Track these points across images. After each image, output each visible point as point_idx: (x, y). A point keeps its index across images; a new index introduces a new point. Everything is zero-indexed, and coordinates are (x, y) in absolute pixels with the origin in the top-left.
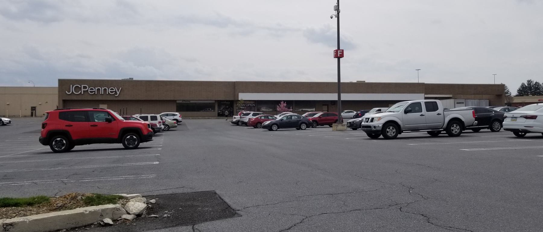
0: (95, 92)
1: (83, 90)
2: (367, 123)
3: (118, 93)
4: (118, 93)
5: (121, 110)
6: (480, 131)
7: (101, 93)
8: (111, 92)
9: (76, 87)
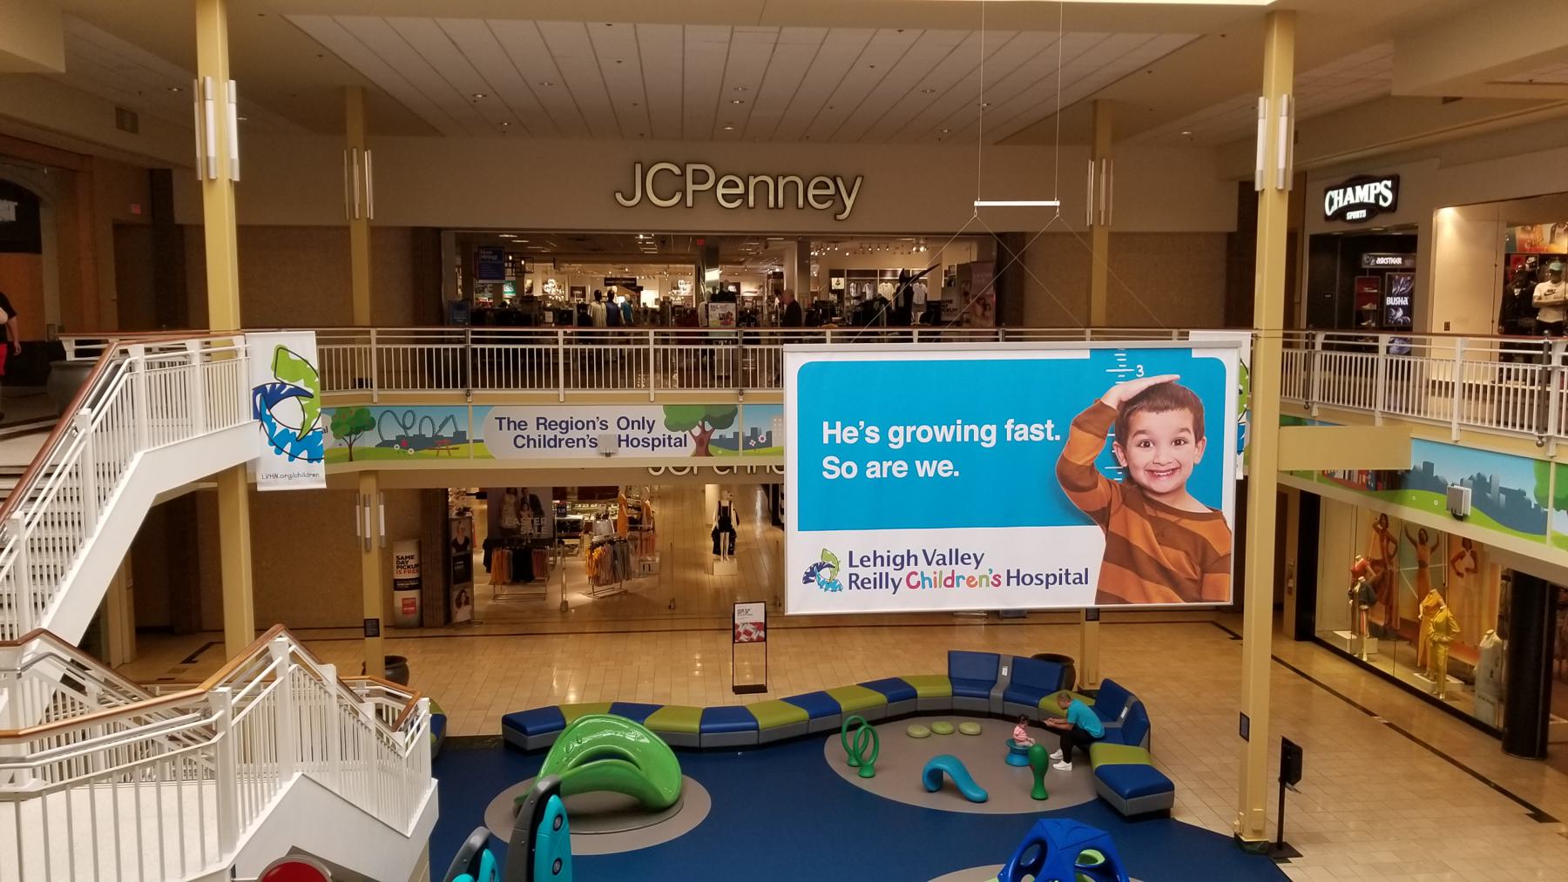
1: (691, 187)
3: (849, 203)
7: (772, 204)
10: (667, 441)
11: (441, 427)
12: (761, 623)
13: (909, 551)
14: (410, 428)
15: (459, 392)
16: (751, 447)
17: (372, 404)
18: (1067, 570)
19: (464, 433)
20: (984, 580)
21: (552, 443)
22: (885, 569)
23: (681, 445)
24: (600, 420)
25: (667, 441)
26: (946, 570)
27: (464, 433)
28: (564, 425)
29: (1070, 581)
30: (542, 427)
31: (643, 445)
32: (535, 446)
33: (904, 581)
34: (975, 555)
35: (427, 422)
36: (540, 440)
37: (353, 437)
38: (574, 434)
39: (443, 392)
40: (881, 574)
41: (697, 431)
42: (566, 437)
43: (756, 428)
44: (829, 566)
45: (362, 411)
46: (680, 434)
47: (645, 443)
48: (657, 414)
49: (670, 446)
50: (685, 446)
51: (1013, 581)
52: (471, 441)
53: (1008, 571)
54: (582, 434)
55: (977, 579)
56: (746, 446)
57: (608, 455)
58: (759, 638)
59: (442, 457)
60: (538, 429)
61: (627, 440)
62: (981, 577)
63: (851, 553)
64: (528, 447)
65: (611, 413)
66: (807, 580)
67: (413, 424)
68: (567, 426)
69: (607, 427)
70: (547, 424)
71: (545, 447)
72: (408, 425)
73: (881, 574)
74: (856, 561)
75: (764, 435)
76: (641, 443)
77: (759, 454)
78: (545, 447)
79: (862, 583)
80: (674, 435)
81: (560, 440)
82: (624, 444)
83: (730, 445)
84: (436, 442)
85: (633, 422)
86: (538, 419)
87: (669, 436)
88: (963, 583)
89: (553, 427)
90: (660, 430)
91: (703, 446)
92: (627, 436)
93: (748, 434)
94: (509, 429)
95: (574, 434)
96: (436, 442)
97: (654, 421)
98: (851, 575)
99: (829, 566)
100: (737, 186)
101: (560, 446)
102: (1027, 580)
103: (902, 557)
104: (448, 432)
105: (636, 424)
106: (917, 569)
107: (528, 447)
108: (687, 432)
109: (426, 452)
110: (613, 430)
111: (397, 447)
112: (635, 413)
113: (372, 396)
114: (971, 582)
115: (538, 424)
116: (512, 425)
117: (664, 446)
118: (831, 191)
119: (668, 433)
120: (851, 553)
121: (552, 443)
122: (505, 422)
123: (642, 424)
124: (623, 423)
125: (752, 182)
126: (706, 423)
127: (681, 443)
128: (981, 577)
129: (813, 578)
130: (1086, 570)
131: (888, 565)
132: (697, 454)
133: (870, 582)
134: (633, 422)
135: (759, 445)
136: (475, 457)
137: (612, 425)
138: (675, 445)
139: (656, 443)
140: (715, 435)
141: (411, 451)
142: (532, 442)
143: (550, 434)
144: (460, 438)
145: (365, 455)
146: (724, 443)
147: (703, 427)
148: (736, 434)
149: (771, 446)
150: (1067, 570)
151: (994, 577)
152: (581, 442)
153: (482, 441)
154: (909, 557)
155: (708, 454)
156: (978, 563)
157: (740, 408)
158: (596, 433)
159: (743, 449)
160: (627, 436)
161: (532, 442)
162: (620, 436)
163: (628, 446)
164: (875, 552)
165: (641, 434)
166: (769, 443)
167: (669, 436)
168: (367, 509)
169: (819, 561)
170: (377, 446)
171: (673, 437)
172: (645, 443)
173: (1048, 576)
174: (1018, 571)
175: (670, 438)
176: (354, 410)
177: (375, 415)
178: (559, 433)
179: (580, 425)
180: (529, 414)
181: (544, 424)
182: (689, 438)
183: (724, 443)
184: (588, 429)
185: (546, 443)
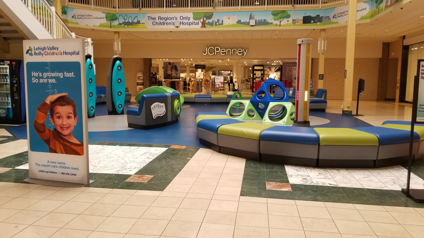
1: (216, 52)
3: (245, 54)
4: (245, 54)
8: (239, 52)
10: (193, 23)
11: (133, 20)
12: (223, 82)
13: (45, 47)
14: (126, 20)
15: (138, 9)
16: (217, 25)
17: (116, 13)
18: (75, 51)
19: (139, 21)
20: (59, 53)
21: (162, 24)
22: (40, 51)
23: (197, 24)
24: (175, 17)
25: (193, 23)
26: (52, 51)
27: (139, 21)
28: (165, 19)
29: (76, 54)
30: (160, 19)
31: (187, 25)
32: (158, 25)
33: (44, 53)
34: (57, 48)
35: (130, 18)
36: (159, 23)
37: (111, 21)
38: (168, 21)
39: (134, 9)
40: (40, 52)
41: (202, 20)
42: (166, 22)
43: (219, 19)
44: (31, 50)
45: (114, 15)
46: (197, 21)
47: (187, 24)
48: (191, 15)
49: (194, 24)
50: (199, 24)
51: (64, 54)
52: (141, 23)
53: (63, 51)
54: (170, 21)
55: (58, 53)
56: (216, 25)
57: (177, 27)
58: (222, 86)
59: (134, 28)
60: (159, 20)
61: (182, 23)
62: (58, 53)
63: (34, 47)
64: (156, 25)
65: (178, 15)
66: (27, 53)
67: (127, 19)
68: (167, 19)
69: (177, 19)
70: (161, 18)
71: (160, 25)
72: (126, 19)
73: (40, 52)
74: (35, 49)
75: (221, 21)
76: (186, 24)
77: (219, 27)
78: (160, 25)
79: (36, 54)
80: (195, 21)
81: (164, 23)
82: (181, 24)
83: (211, 24)
84: (132, 24)
85: (184, 18)
86: (159, 17)
87: (194, 22)
88: (55, 54)
89: (163, 19)
90: (192, 20)
91: (204, 24)
92: (183, 22)
93: (216, 21)
94: (151, 20)
95: (168, 21)
96: (132, 24)
97: (190, 18)
98: (34, 52)
99: (31, 50)
100: (224, 51)
101: (164, 25)
102: (67, 54)
103: (43, 48)
104: (135, 21)
105: (185, 18)
106: (46, 51)
107: (156, 25)
108: (199, 21)
109: (130, 26)
110: (179, 20)
111: (123, 25)
112: (185, 15)
113: (116, 11)
114: (56, 54)
115: (159, 18)
116: (152, 19)
117: (193, 24)
118: (242, 51)
119: (194, 21)
120: (34, 47)
121: (162, 24)
122: (150, 18)
123: (187, 18)
124: (181, 18)
125: (227, 50)
126: (204, 18)
127: (197, 24)
128: (58, 53)
129: (28, 53)
130: (79, 51)
131: (41, 50)
132: (202, 27)
133: (38, 54)
134: (184, 18)
135: (219, 24)
136: (142, 28)
137: (178, 18)
138: (196, 24)
139: (190, 24)
140: (207, 21)
141: (126, 26)
142: (157, 24)
143: (162, 21)
144: (139, 22)
145: (115, 27)
146: (209, 24)
147: (203, 19)
148: (213, 21)
149: (223, 24)
150: (75, 51)
151: (61, 53)
152: (170, 24)
153: (144, 23)
154: (45, 48)
155: (205, 27)
156: (58, 49)
157: (214, 13)
158: (173, 21)
159: (215, 25)
160: (183, 22)
161: (157, 24)
162: (180, 22)
163: (183, 25)
164: (38, 47)
165: (186, 21)
166: (222, 24)
167: (194, 22)
168: (323, 49)
169: (29, 49)
170: (118, 24)
171: (195, 22)
172: (187, 24)
173: (71, 53)
174: (65, 51)
175: (194, 22)
176: (112, 14)
177: (117, 16)
178: (164, 21)
179: (170, 19)
180: (156, 16)
181: (160, 18)
182: (200, 22)
183: (209, 24)
184: (172, 20)
185: (160, 24)
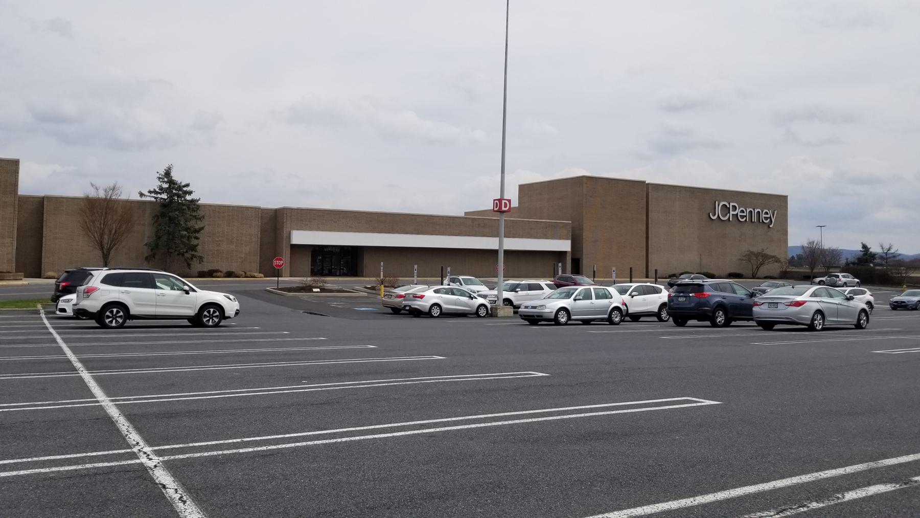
0: (746, 216)
2: (587, 302)
5: (442, 267)
6: (640, 320)
9: (724, 205)
